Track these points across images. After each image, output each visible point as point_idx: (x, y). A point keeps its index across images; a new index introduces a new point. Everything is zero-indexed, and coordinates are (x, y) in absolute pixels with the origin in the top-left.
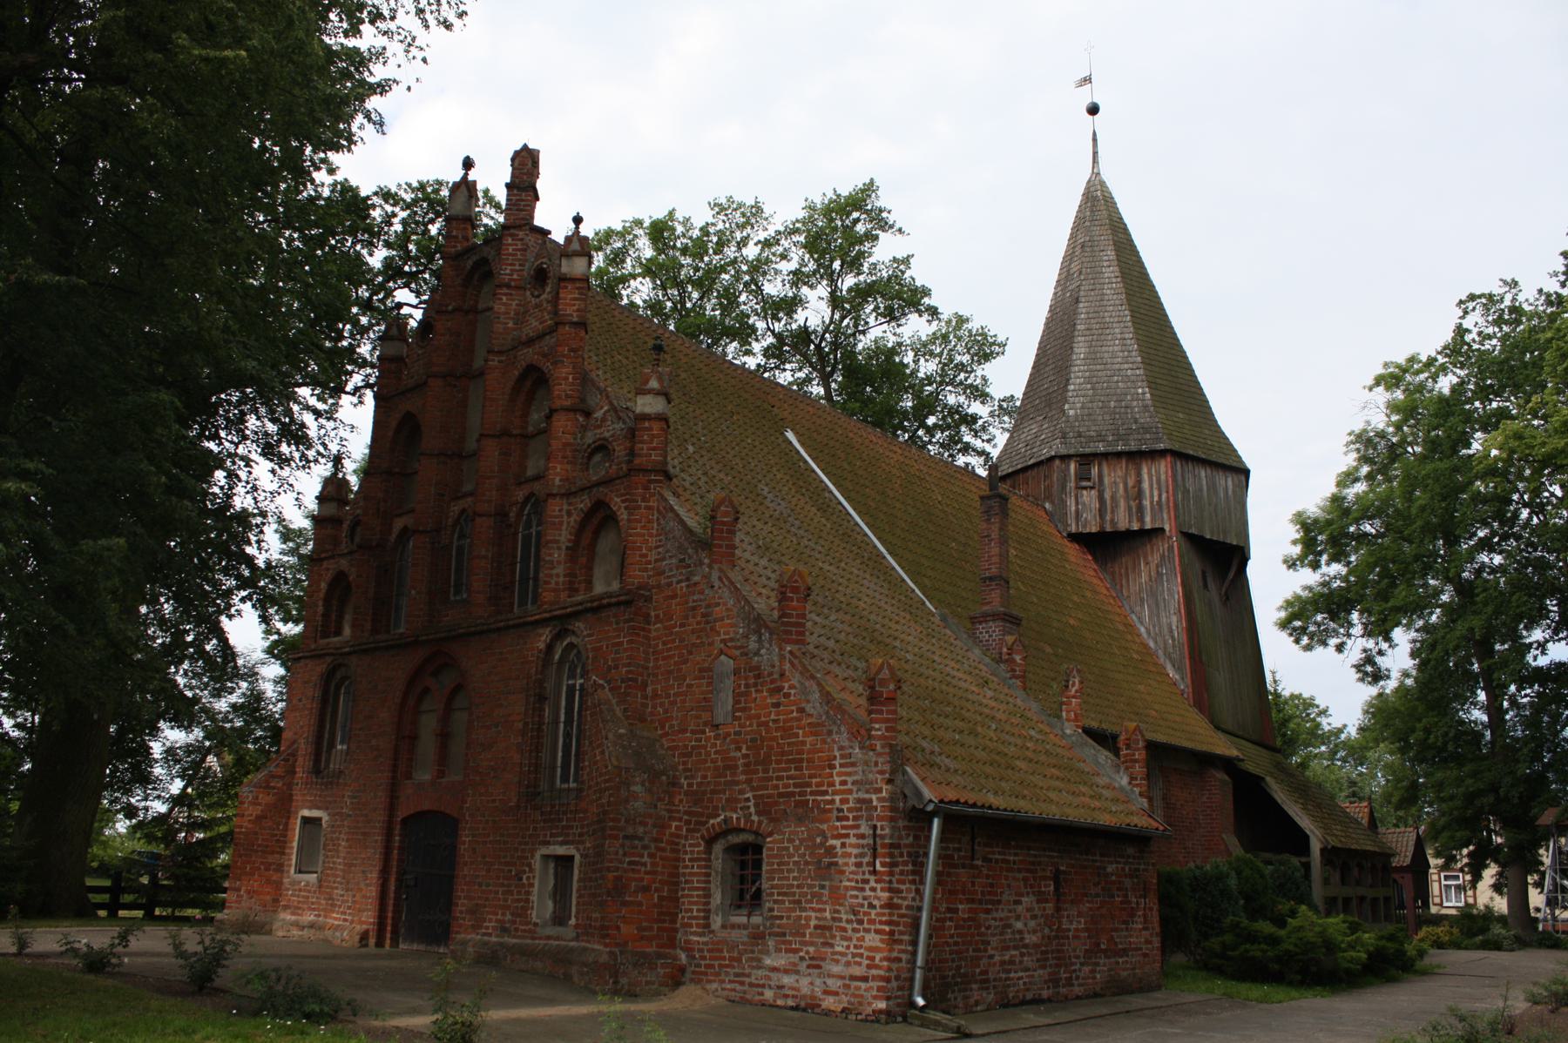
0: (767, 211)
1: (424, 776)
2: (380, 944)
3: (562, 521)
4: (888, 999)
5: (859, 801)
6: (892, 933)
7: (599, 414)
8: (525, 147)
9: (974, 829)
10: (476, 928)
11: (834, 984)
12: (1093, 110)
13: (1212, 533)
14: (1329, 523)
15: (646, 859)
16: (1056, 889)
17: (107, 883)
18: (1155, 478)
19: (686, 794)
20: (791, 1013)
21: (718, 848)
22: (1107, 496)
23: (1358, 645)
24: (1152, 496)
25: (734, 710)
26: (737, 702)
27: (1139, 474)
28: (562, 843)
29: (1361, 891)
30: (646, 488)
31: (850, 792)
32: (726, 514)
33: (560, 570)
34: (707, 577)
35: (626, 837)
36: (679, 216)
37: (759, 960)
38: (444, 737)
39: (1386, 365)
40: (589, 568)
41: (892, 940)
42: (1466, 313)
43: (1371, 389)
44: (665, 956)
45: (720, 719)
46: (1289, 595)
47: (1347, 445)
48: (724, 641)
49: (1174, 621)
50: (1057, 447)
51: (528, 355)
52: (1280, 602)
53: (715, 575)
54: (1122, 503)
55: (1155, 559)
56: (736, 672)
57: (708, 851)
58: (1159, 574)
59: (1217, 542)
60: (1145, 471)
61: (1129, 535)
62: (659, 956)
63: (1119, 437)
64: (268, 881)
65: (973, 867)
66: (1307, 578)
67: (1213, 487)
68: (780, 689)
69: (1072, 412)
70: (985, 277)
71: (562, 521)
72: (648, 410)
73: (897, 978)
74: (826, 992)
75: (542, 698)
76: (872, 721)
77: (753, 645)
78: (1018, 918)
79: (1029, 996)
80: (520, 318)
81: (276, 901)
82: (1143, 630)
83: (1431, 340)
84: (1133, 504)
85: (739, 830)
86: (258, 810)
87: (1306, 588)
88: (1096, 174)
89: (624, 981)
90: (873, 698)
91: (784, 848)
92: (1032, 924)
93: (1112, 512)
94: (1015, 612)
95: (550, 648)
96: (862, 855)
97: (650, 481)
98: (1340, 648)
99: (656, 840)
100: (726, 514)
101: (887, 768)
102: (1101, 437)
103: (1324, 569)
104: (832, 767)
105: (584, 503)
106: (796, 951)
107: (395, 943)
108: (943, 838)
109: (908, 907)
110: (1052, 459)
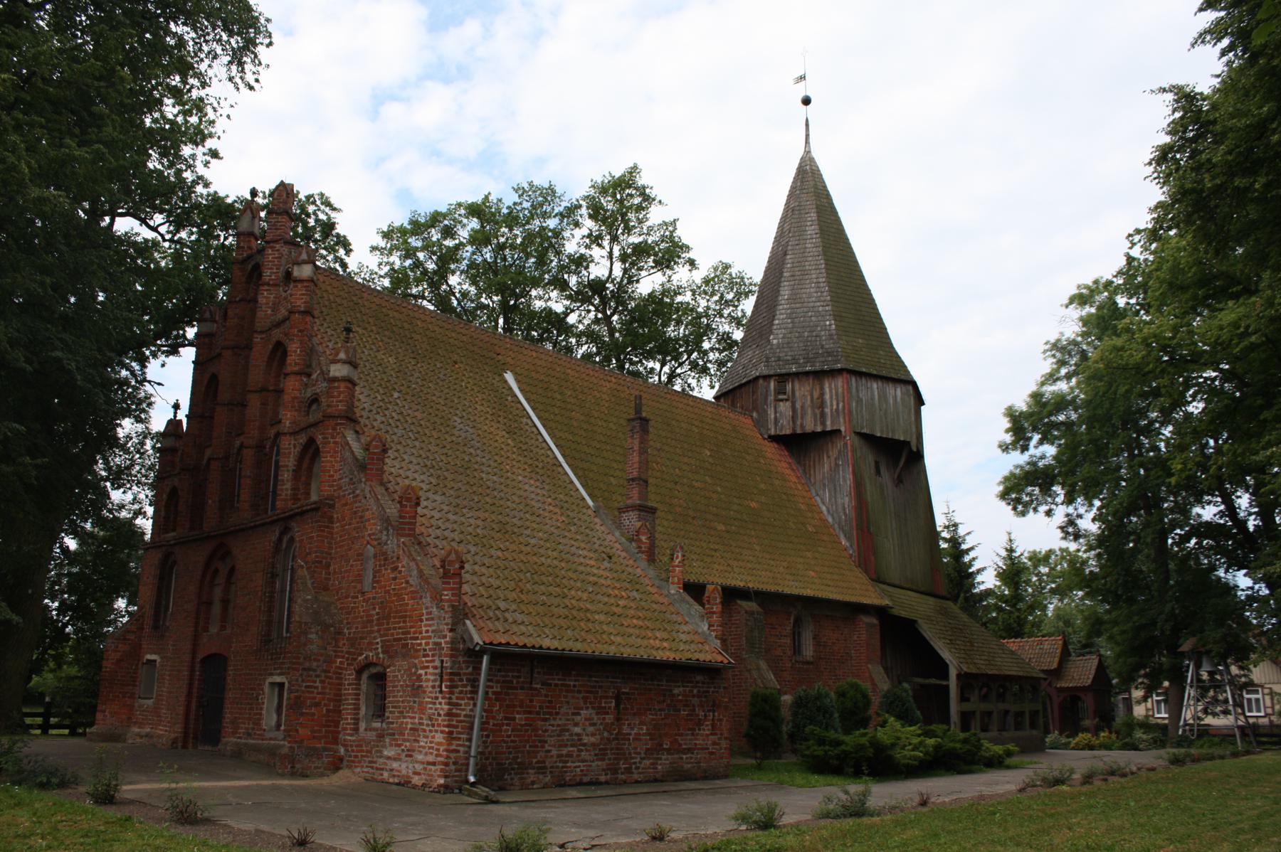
0: (559, 191)
1: (214, 630)
3: (290, 449)
4: (446, 777)
5: (435, 644)
6: (450, 733)
7: (314, 376)
8: (282, 183)
9: (509, 660)
10: (234, 733)
11: (419, 767)
12: (806, 101)
13: (882, 431)
15: (318, 684)
16: (617, 705)
17: (41, 710)
18: (832, 390)
19: (348, 639)
20: (395, 787)
21: (365, 676)
22: (798, 406)
23: (1061, 513)
25: (374, 582)
26: (374, 577)
27: (822, 389)
28: (280, 674)
29: (1002, 706)
30: (334, 429)
31: (430, 637)
32: (376, 447)
33: (288, 486)
34: (363, 491)
35: (304, 669)
36: (493, 198)
37: (381, 752)
38: (225, 602)
39: (1079, 287)
40: (308, 484)
41: (450, 737)
42: (1133, 244)
43: (1067, 307)
45: (366, 589)
46: (1006, 473)
47: (1045, 352)
48: (370, 535)
49: (846, 501)
50: (763, 369)
51: (277, 334)
52: (1000, 479)
53: (368, 489)
54: (809, 411)
55: (834, 453)
56: (375, 556)
57: (359, 678)
58: (837, 465)
60: (827, 385)
61: (814, 436)
62: (325, 749)
65: (531, 689)
66: (1018, 459)
67: (883, 396)
68: (396, 568)
70: (726, 233)
71: (290, 449)
72: (338, 374)
73: (454, 763)
74: (415, 773)
75: (274, 575)
76: (445, 589)
77: (384, 538)
78: (576, 725)
79: (586, 779)
80: (275, 308)
81: (129, 718)
82: (824, 508)
83: (1108, 266)
84: (818, 412)
85: (375, 665)
87: (1016, 467)
88: (808, 152)
89: (298, 766)
90: (446, 575)
91: (397, 673)
92: (591, 729)
93: (802, 418)
94: (650, 504)
95: (280, 540)
96: (435, 680)
98: (1049, 513)
99: (325, 671)
100: (376, 447)
101: (450, 621)
102: (795, 361)
103: (1032, 451)
104: (421, 621)
105: (303, 439)
106: (399, 745)
108: (489, 669)
110: (757, 378)
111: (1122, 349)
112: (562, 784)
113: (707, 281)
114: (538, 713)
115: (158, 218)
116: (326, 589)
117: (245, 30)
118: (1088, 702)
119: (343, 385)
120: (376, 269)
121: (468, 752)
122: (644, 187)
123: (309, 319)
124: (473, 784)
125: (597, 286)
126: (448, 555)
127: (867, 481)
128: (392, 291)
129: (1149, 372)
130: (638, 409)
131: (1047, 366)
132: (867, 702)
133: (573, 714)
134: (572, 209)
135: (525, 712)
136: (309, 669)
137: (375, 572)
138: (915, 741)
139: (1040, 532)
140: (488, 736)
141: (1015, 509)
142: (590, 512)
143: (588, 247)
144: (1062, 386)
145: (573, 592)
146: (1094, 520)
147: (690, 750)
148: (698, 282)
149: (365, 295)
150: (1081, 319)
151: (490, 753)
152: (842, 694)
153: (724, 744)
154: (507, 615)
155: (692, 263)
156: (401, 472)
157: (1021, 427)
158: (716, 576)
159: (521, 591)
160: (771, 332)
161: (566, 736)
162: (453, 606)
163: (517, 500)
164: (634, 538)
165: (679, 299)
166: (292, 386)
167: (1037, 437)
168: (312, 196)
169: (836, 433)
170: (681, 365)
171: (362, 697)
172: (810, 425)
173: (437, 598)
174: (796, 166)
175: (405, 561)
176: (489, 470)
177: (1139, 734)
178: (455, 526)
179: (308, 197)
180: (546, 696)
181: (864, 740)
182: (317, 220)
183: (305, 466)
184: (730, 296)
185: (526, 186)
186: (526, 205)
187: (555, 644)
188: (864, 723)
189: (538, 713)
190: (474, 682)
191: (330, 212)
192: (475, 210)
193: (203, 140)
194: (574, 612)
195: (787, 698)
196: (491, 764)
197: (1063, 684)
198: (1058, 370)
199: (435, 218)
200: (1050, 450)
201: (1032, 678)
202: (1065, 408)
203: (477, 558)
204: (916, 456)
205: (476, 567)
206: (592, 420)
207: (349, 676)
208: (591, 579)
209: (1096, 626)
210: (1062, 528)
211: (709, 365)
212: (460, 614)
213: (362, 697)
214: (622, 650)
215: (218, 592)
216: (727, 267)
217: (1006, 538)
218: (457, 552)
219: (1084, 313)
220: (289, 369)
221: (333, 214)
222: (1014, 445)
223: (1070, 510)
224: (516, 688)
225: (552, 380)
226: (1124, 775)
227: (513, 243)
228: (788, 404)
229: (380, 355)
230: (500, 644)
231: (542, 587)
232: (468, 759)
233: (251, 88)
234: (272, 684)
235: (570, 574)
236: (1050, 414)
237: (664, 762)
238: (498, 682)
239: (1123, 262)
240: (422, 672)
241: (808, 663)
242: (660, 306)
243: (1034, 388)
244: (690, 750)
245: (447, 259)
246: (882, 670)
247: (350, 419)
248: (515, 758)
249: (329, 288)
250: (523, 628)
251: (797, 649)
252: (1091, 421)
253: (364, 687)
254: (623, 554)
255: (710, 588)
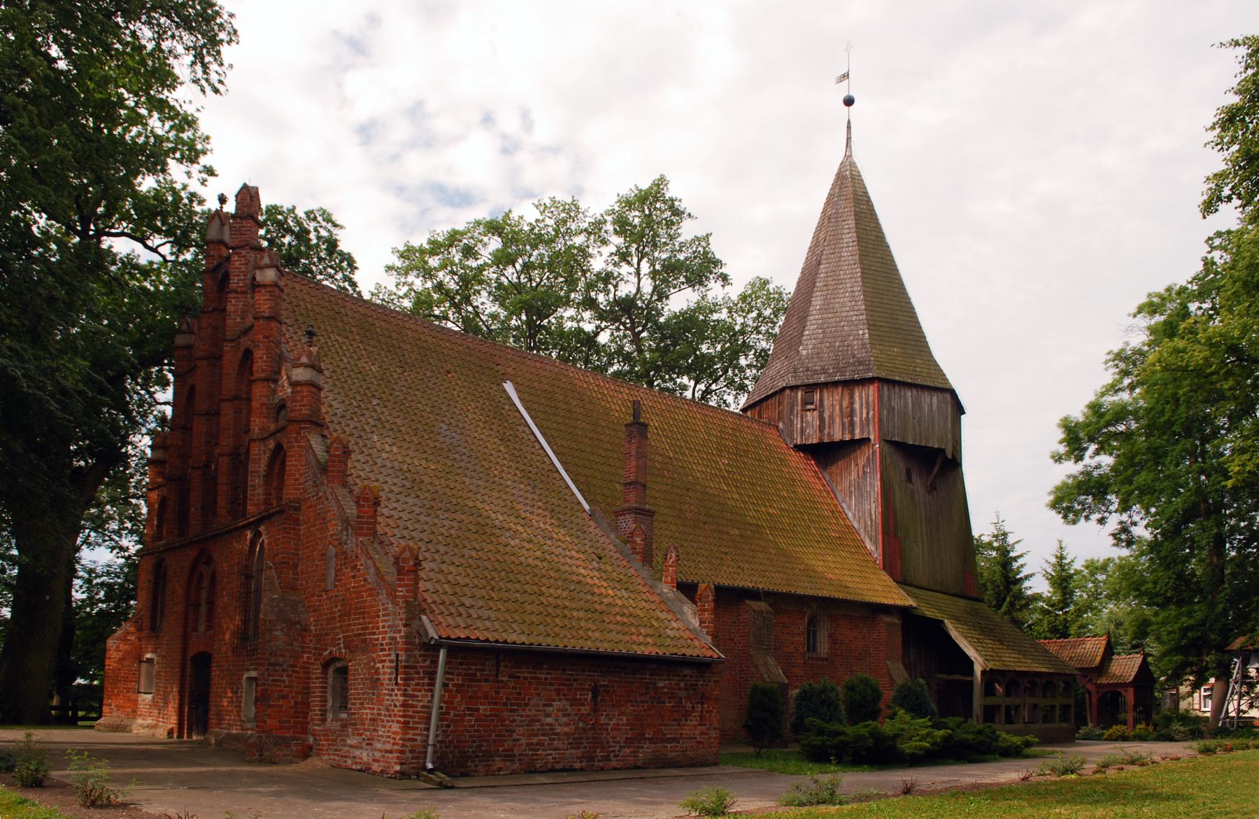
0: (583, 206)
2: (180, 736)
4: (401, 764)
5: (392, 638)
9: (462, 651)
10: (219, 724)
11: (378, 755)
12: (849, 102)
13: (915, 440)
14: (1088, 425)
16: (594, 698)
18: (864, 399)
21: (331, 670)
22: (826, 415)
23: (1114, 521)
24: (861, 413)
27: (852, 397)
30: (298, 433)
31: (386, 632)
32: (337, 449)
33: (260, 491)
35: (270, 664)
36: (515, 216)
39: (1149, 295)
41: (406, 726)
44: (298, 739)
47: (1106, 362)
49: (873, 507)
51: (246, 342)
52: (1050, 488)
53: (329, 490)
54: (838, 420)
56: (336, 556)
59: (919, 447)
61: (842, 444)
62: (294, 739)
63: (838, 369)
64: (129, 700)
66: (1071, 468)
67: (918, 405)
69: (804, 352)
70: (760, 244)
72: (300, 378)
73: (411, 751)
74: (375, 760)
77: (344, 538)
78: (548, 715)
79: (558, 766)
81: (134, 711)
82: (850, 515)
85: (339, 659)
86: (120, 655)
87: (1069, 477)
88: (848, 157)
89: (267, 754)
90: (400, 571)
91: (357, 666)
92: (565, 719)
94: (647, 507)
97: (301, 428)
98: (1102, 521)
100: (337, 449)
102: (824, 371)
103: (1087, 460)
105: (272, 444)
107: (190, 735)
108: (447, 663)
109: (423, 707)
110: (783, 389)
111: (1184, 351)
112: (531, 770)
113: (744, 298)
114: (505, 704)
115: (156, 240)
116: (294, 588)
117: (207, 29)
118: (1129, 697)
119: (305, 389)
120: (395, 290)
121: (426, 741)
122: (672, 200)
123: (274, 324)
124: (431, 771)
125: (626, 306)
126: (402, 553)
127: (896, 487)
128: (415, 311)
129: (1212, 374)
130: (636, 415)
131: (1108, 377)
132: (877, 695)
133: (545, 705)
134: (598, 224)
135: (490, 704)
136: (275, 664)
137: (337, 571)
138: (924, 732)
139: (1093, 542)
140: (448, 726)
141: (1065, 517)
142: (585, 515)
143: (615, 264)
144: (1125, 396)
145: (552, 591)
146: (1146, 527)
147: (674, 740)
148: (735, 298)
149: (349, 305)
150: (1149, 328)
151: (451, 742)
152: (851, 688)
153: (713, 734)
154: (471, 611)
155: (725, 278)
156: (371, 475)
157: (1075, 439)
158: (709, 577)
159: (492, 589)
160: (800, 343)
161: (537, 726)
162: (407, 602)
163: (502, 504)
164: (629, 539)
165: (715, 316)
166: (259, 391)
167: (1093, 447)
168: (312, 212)
169: (866, 441)
170: (715, 381)
171: (329, 690)
172: (838, 435)
173: (392, 595)
174: (836, 171)
175: (363, 559)
176: (474, 474)
177: (1176, 726)
178: (426, 527)
179: (307, 214)
180: (514, 688)
181: (864, 731)
182: (319, 238)
183: (276, 471)
184: (767, 312)
185: (548, 203)
186: (551, 222)
187: (523, 639)
188: (874, 715)
189: (505, 704)
190: (432, 675)
191: (332, 229)
192: (494, 228)
193: (197, 157)
194: (550, 609)
195: (795, 692)
196: (452, 752)
197: (1104, 681)
198: (1120, 381)
199: (454, 237)
200: (1107, 460)
201: (1065, 674)
202: (1124, 419)
203: (445, 558)
204: (953, 464)
205: (444, 567)
206: (599, 429)
207: (317, 670)
208: (575, 578)
209: (1142, 629)
210: (1114, 535)
211: (746, 382)
212: (415, 609)
213: (329, 690)
214: (635, 647)
215: (204, 594)
216: (766, 283)
217: (1056, 546)
218: (411, 550)
219: (1153, 322)
220: (256, 375)
221: (335, 231)
222: (1068, 456)
223: (1125, 517)
224: (480, 681)
225: (557, 390)
226: (1143, 765)
227: (542, 264)
228: (816, 413)
229: (361, 364)
230: (459, 638)
231: (517, 586)
232: (426, 747)
233: (216, 91)
234: (250, 679)
235: (552, 573)
236: (1108, 424)
237: (646, 750)
238: (458, 675)
239: (1199, 267)
240: (379, 665)
241: (823, 659)
242: (692, 325)
243: (1091, 398)
244: (674, 740)
245: (470, 281)
246: (901, 666)
247: (316, 423)
248: (480, 747)
249: (306, 297)
250: (488, 624)
251: (812, 646)
252: (1150, 429)
253: (330, 680)
254: (618, 555)
255: (702, 586)
